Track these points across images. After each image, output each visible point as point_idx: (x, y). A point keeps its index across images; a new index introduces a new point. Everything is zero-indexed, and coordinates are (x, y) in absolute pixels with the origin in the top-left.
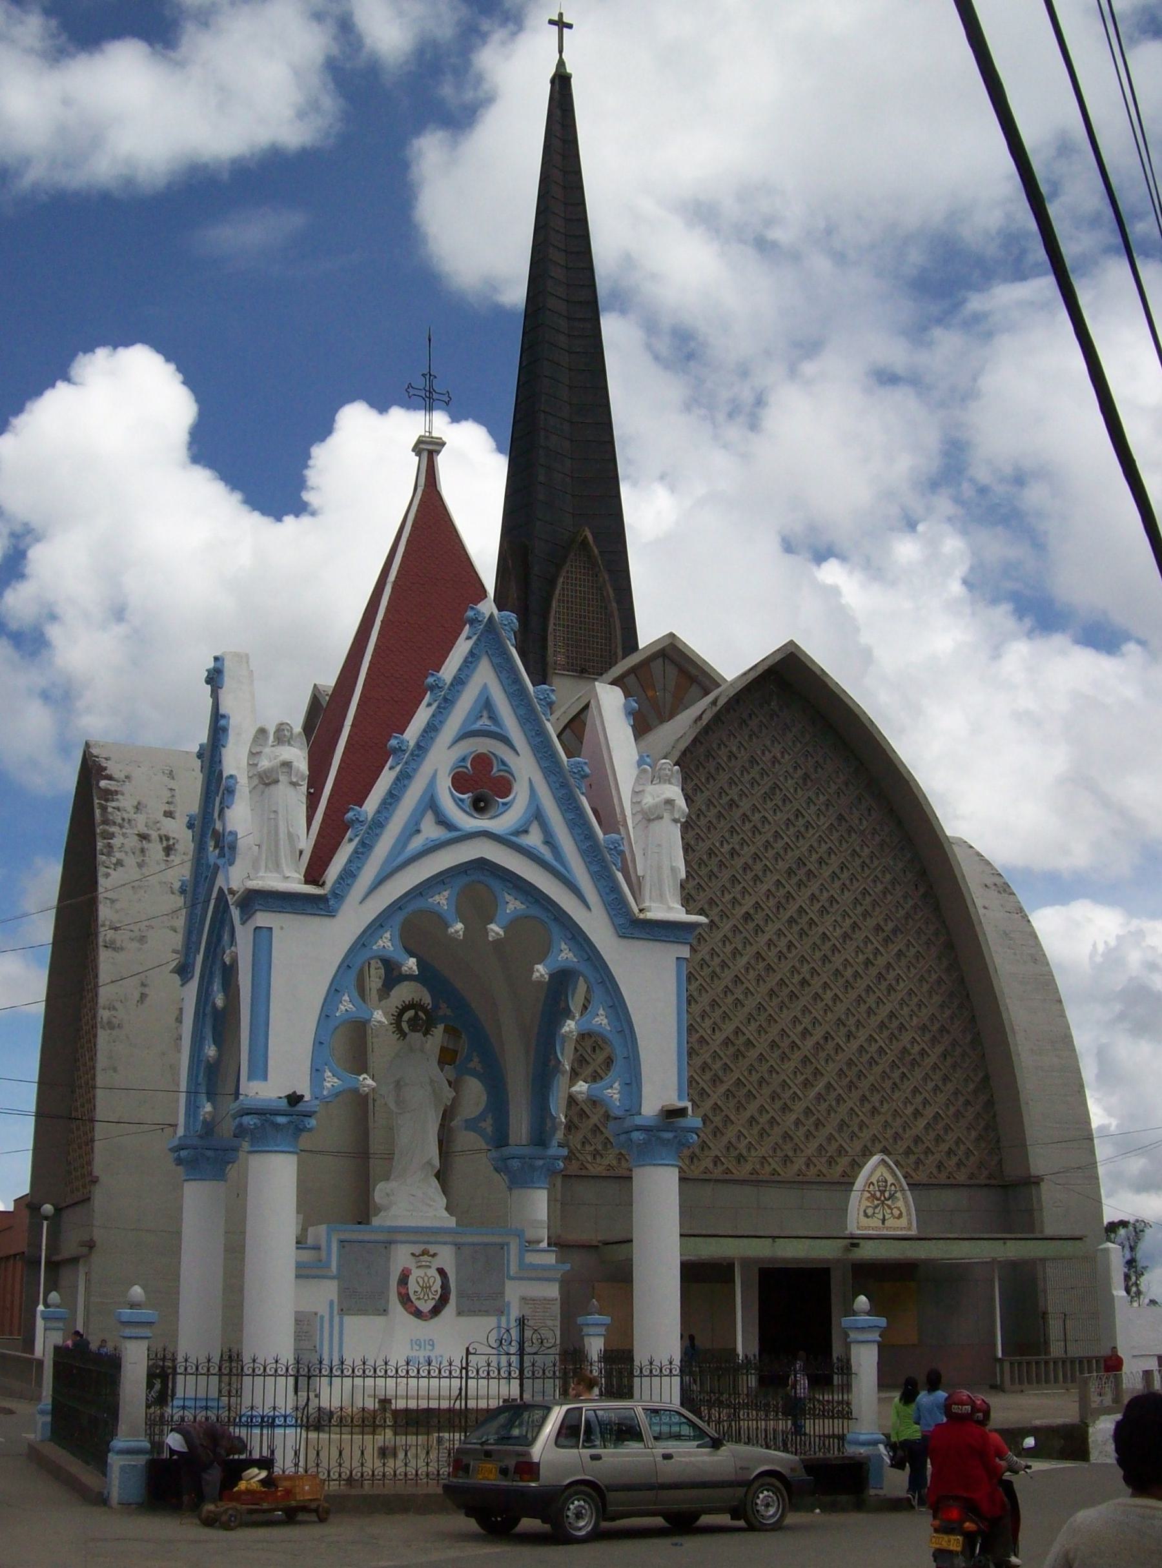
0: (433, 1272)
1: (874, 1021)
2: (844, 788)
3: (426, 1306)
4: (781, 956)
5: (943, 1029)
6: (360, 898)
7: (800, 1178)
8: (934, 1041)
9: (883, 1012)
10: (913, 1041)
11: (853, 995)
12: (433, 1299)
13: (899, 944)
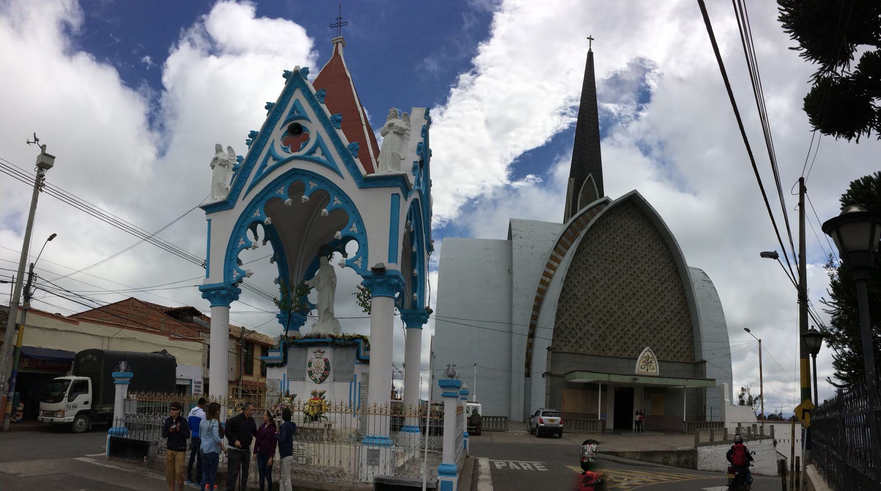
0: (322, 361)
1: (656, 308)
2: (651, 236)
3: (318, 376)
4: (627, 286)
5: (678, 312)
6: (339, 178)
7: (629, 357)
8: (675, 316)
9: (660, 305)
10: (668, 315)
11: (650, 299)
12: (321, 373)
13: (666, 285)
